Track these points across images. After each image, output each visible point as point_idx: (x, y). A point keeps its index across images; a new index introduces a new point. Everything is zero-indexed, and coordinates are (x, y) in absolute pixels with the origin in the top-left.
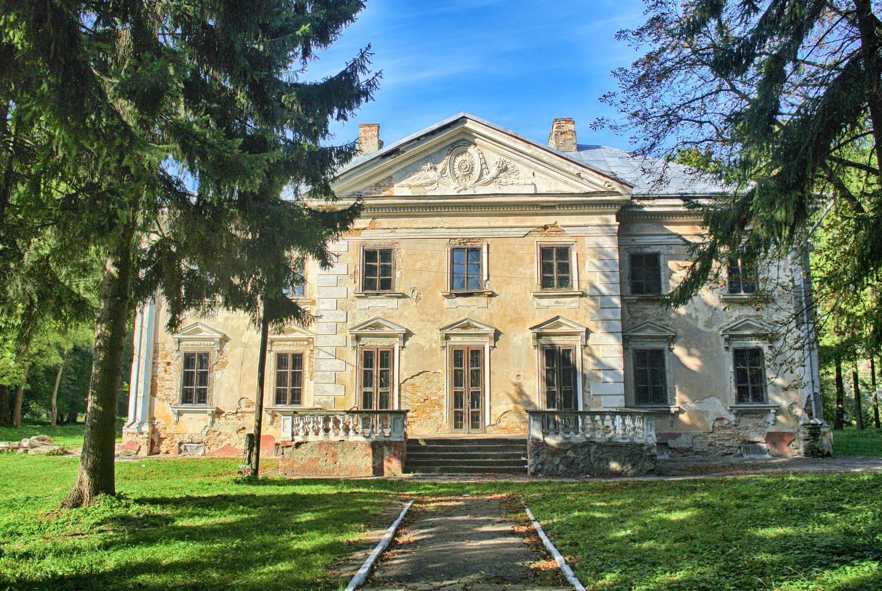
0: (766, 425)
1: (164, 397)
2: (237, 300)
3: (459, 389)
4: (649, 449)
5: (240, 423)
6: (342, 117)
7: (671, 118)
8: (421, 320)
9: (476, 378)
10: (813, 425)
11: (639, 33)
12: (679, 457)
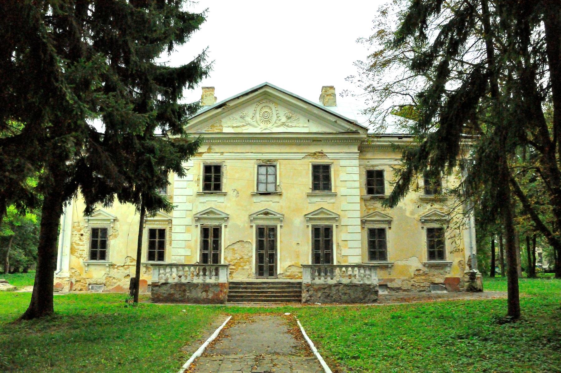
0: (445, 273)
1: (79, 256)
2: (125, 197)
3: (261, 252)
4: (374, 287)
5: (127, 272)
6: (191, 87)
7: (387, 91)
8: (237, 211)
9: (273, 245)
10: (471, 273)
11: (371, 39)
12: (393, 293)
